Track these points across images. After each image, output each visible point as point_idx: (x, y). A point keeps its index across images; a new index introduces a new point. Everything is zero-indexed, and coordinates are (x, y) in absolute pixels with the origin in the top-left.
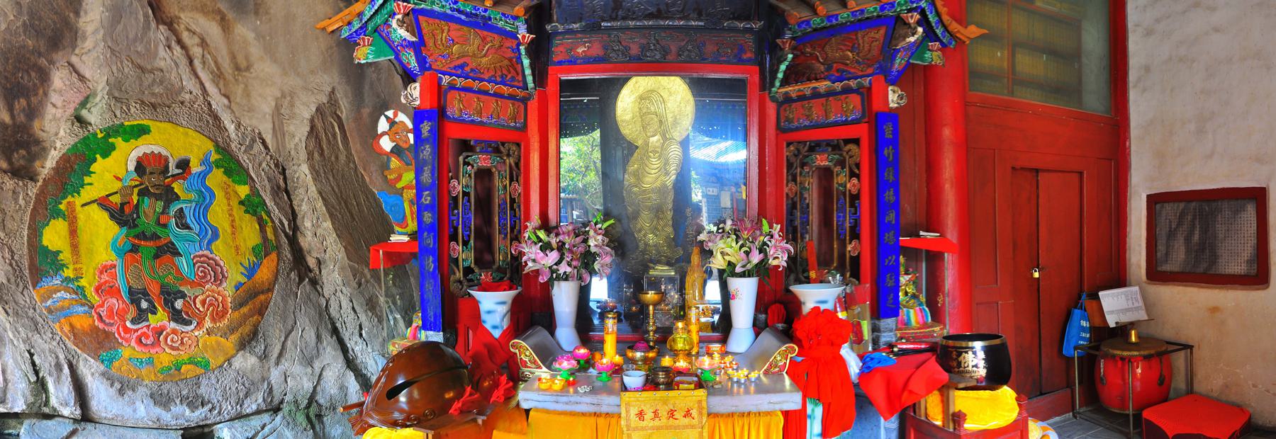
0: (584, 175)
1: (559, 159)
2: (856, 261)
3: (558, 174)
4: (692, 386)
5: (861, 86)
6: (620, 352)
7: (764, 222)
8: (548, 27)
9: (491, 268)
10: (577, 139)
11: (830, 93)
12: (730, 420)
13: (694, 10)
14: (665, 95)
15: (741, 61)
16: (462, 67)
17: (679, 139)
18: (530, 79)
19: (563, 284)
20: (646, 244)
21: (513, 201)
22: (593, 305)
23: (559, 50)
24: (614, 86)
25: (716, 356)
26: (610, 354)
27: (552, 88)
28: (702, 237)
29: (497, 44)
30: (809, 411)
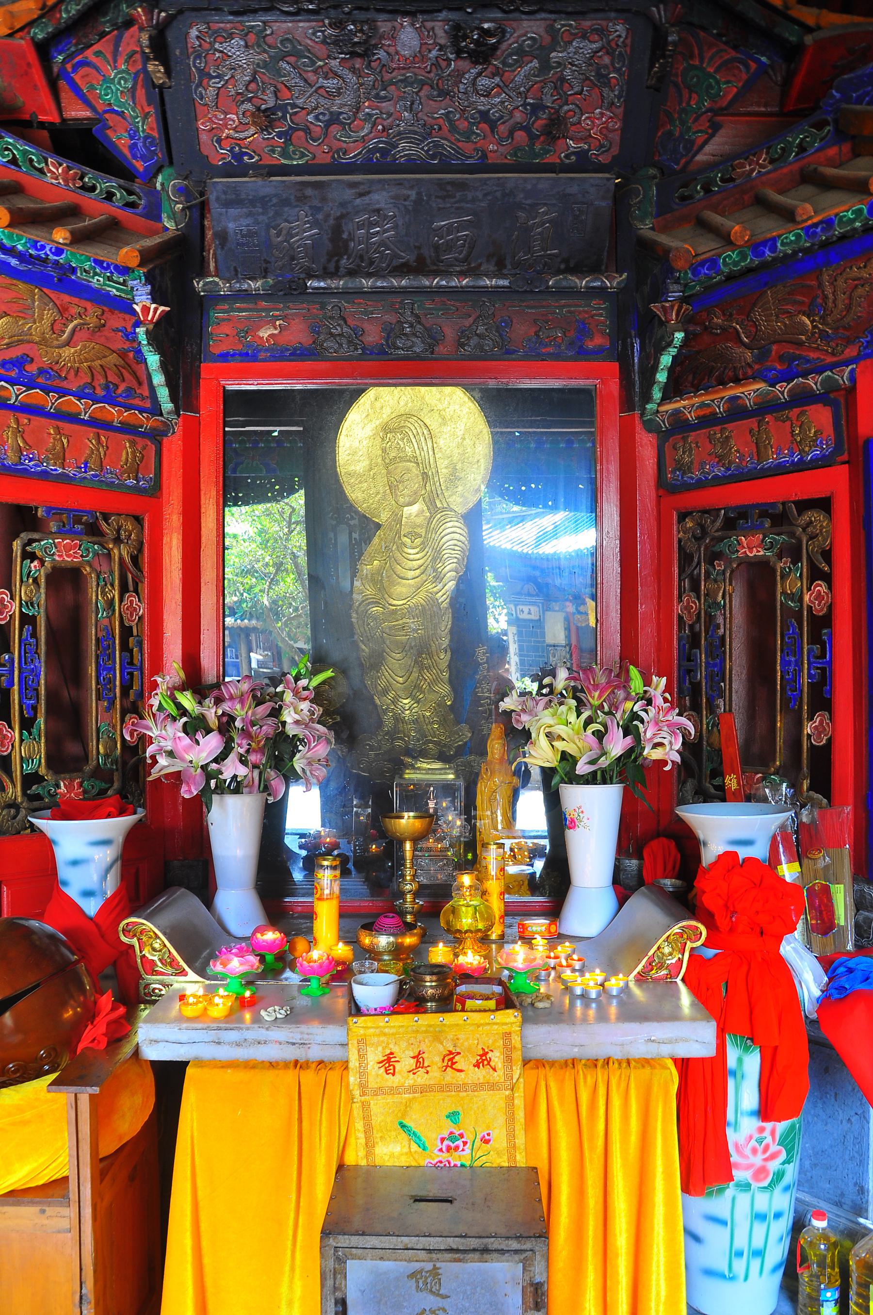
0: (273, 582)
1: (222, 548)
2: (822, 758)
3: (221, 578)
4: (492, 1004)
5: (831, 387)
6: (347, 936)
7: (634, 672)
8: (199, 285)
9: (80, 770)
10: (259, 508)
11: (767, 407)
12: (568, 1074)
13: (489, 258)
14: (433, 422)
15: (582, 353)
16: (20, 363)
17: (461, 510)
18: (163, 393)
19: (231, 800)
20: (398, 719)
21: (126, 632)
22: (292, 843)
23: (222, 330)
24: (332, 406)
25: (540, 942)
26: (327, 942)
27: (209, 408)
28: (509, 703)
29: (91, 320)
30: (731, 1061)
